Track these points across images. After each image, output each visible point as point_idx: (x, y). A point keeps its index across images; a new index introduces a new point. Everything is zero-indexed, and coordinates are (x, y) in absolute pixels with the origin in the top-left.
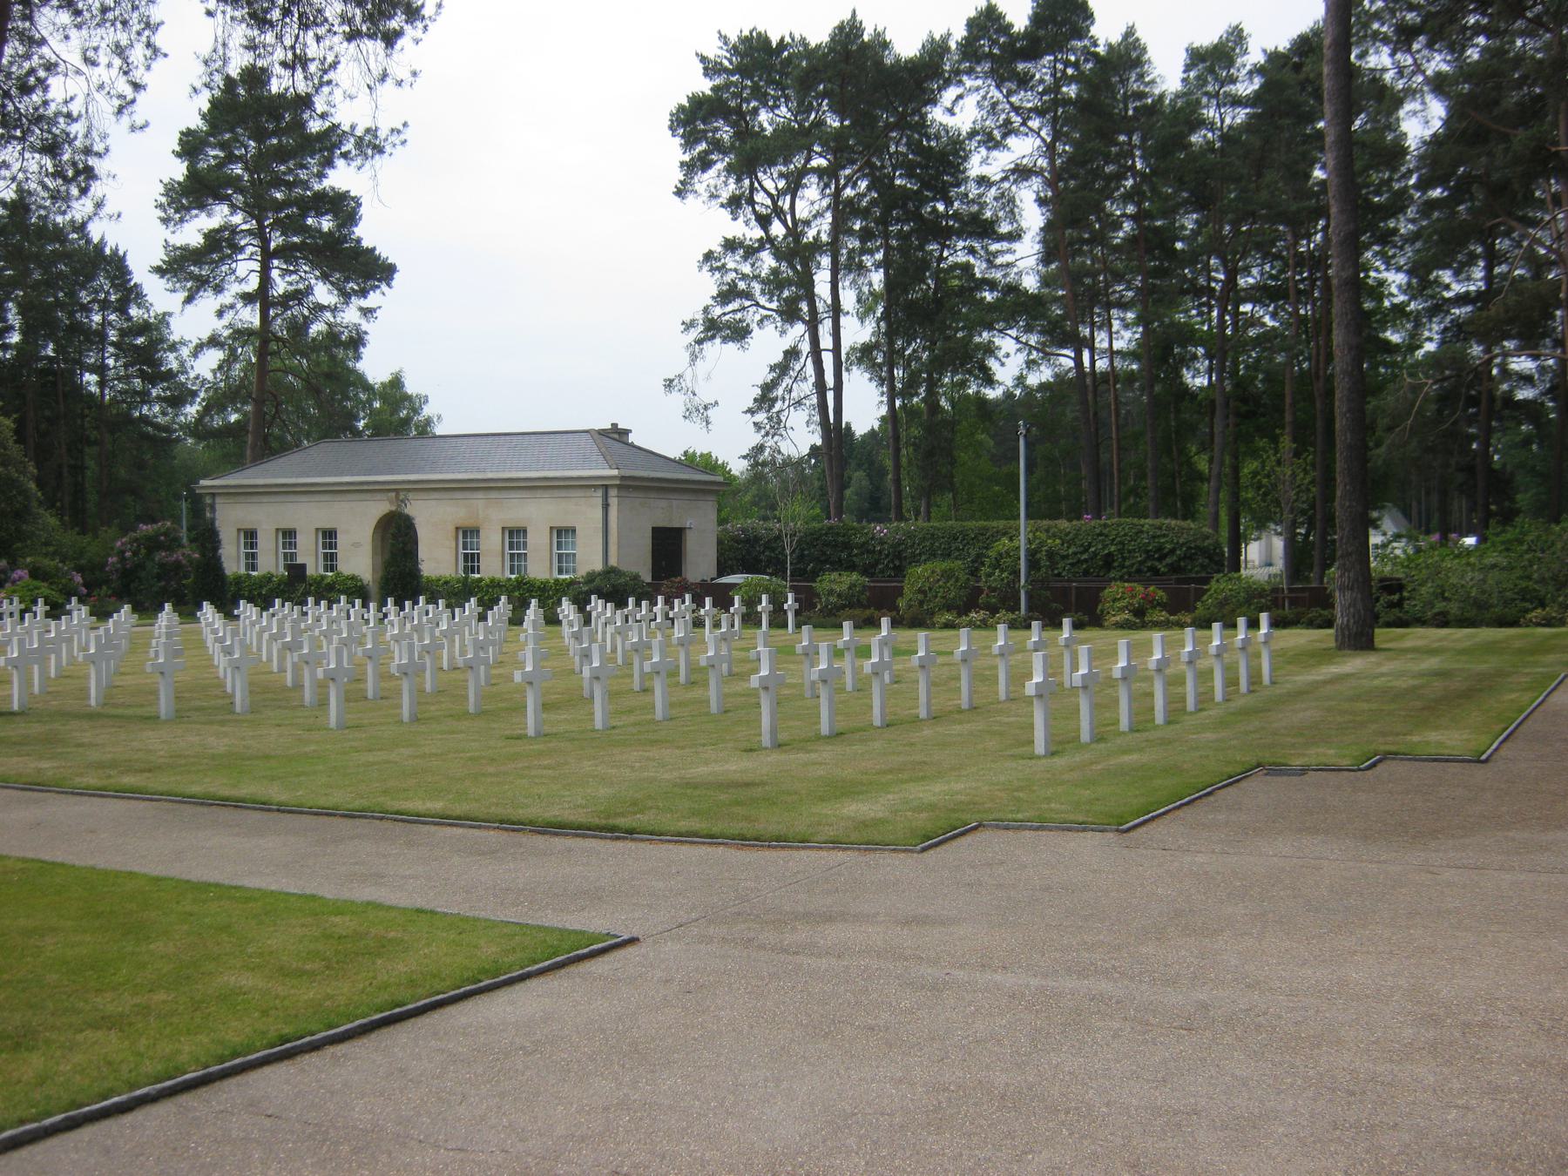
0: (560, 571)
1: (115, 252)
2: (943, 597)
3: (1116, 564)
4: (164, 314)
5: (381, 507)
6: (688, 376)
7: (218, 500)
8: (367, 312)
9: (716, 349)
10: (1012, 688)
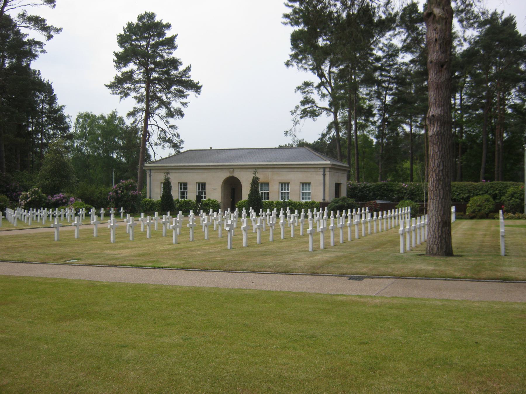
0: (303, 199)
1: (48, 83)
2: (489, 208)
3: (498, 197)
4: (62, 106)
5: (225, 175)
6: (293, 130)
7: (152, 171)
8: (183, 104)
9: (308, 120)
10: (335, 239)
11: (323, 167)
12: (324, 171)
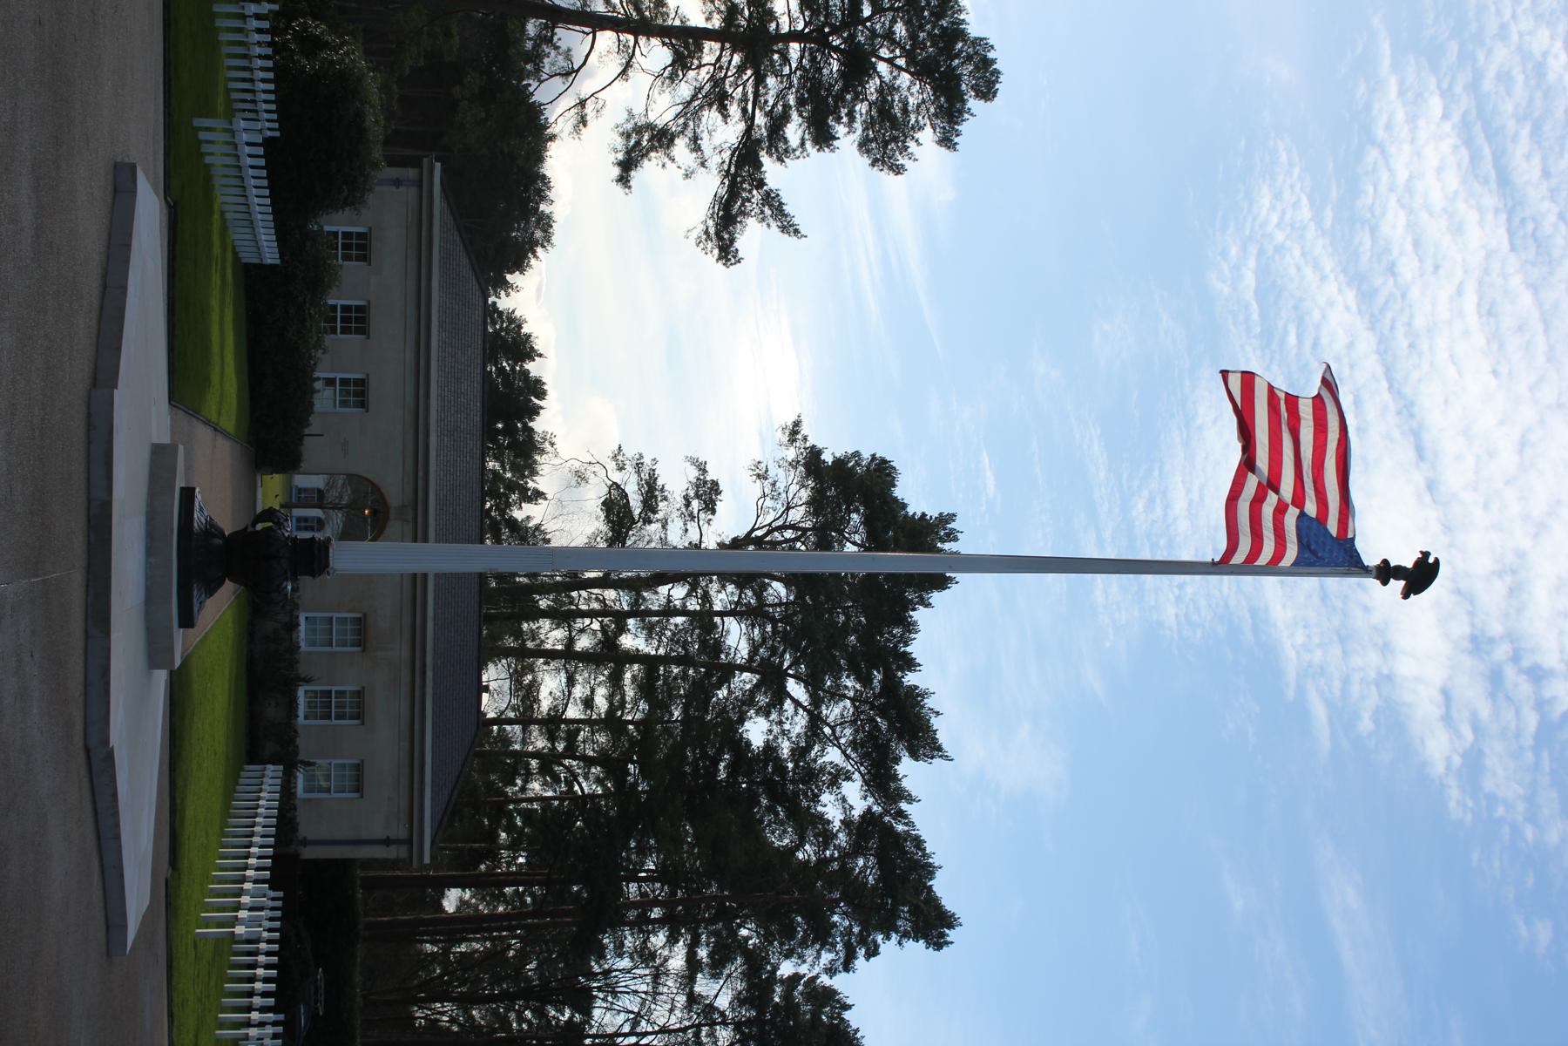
11: (421, 181)
12: (398, 842)
